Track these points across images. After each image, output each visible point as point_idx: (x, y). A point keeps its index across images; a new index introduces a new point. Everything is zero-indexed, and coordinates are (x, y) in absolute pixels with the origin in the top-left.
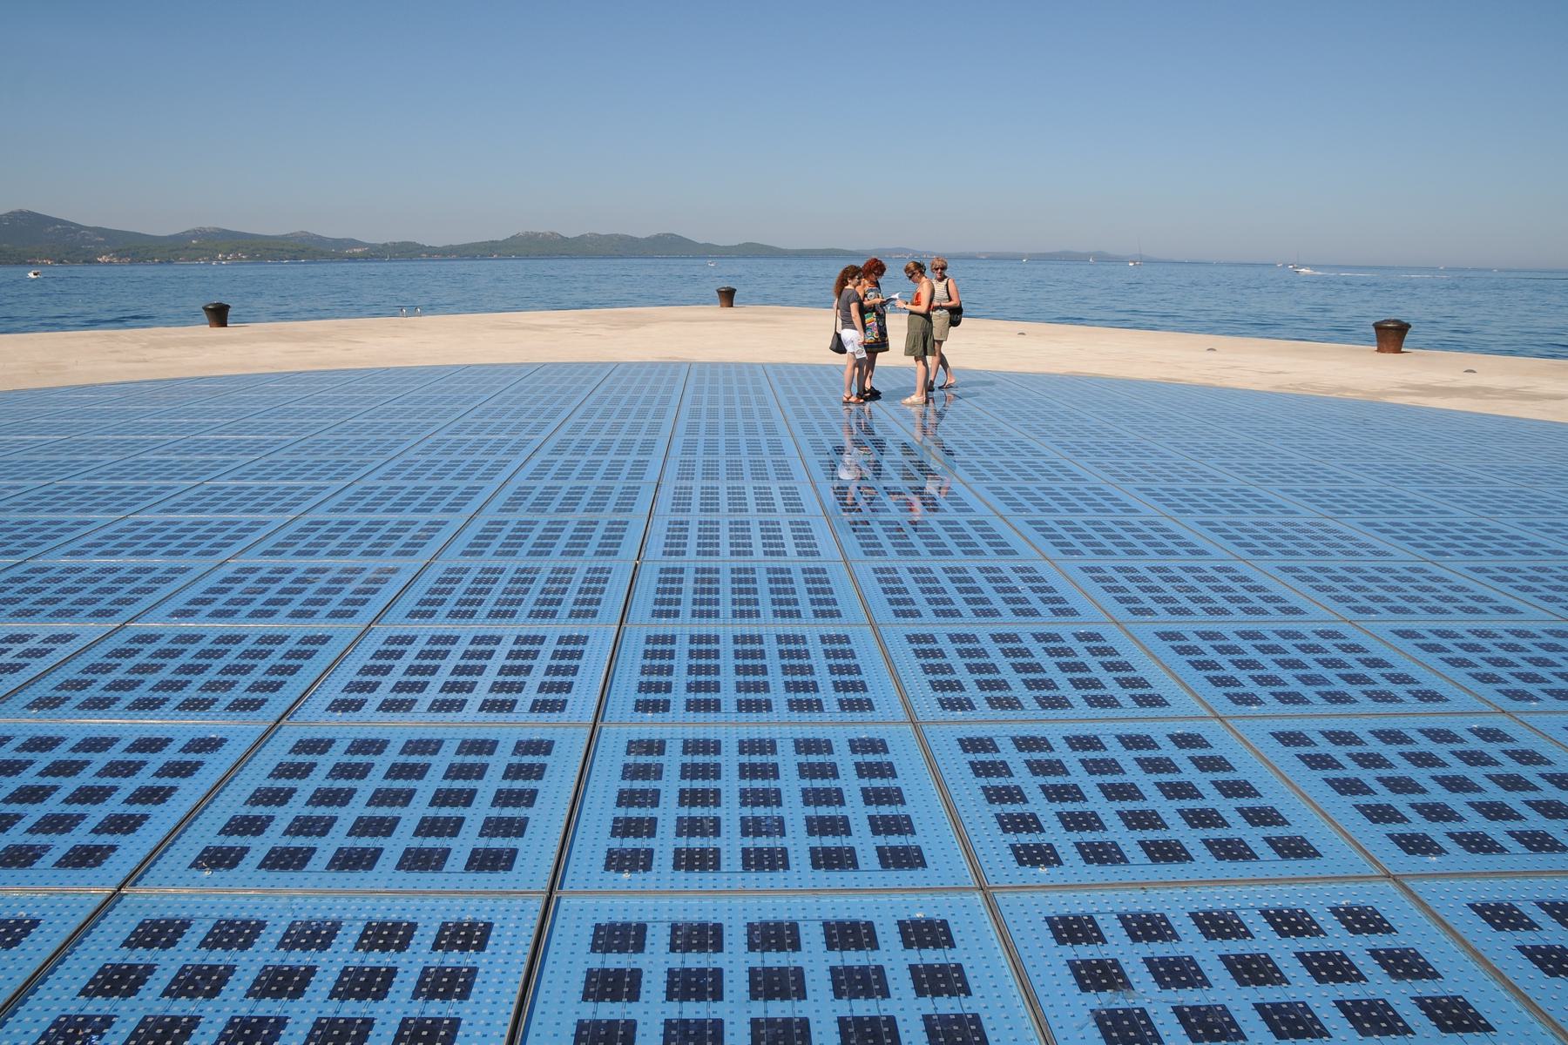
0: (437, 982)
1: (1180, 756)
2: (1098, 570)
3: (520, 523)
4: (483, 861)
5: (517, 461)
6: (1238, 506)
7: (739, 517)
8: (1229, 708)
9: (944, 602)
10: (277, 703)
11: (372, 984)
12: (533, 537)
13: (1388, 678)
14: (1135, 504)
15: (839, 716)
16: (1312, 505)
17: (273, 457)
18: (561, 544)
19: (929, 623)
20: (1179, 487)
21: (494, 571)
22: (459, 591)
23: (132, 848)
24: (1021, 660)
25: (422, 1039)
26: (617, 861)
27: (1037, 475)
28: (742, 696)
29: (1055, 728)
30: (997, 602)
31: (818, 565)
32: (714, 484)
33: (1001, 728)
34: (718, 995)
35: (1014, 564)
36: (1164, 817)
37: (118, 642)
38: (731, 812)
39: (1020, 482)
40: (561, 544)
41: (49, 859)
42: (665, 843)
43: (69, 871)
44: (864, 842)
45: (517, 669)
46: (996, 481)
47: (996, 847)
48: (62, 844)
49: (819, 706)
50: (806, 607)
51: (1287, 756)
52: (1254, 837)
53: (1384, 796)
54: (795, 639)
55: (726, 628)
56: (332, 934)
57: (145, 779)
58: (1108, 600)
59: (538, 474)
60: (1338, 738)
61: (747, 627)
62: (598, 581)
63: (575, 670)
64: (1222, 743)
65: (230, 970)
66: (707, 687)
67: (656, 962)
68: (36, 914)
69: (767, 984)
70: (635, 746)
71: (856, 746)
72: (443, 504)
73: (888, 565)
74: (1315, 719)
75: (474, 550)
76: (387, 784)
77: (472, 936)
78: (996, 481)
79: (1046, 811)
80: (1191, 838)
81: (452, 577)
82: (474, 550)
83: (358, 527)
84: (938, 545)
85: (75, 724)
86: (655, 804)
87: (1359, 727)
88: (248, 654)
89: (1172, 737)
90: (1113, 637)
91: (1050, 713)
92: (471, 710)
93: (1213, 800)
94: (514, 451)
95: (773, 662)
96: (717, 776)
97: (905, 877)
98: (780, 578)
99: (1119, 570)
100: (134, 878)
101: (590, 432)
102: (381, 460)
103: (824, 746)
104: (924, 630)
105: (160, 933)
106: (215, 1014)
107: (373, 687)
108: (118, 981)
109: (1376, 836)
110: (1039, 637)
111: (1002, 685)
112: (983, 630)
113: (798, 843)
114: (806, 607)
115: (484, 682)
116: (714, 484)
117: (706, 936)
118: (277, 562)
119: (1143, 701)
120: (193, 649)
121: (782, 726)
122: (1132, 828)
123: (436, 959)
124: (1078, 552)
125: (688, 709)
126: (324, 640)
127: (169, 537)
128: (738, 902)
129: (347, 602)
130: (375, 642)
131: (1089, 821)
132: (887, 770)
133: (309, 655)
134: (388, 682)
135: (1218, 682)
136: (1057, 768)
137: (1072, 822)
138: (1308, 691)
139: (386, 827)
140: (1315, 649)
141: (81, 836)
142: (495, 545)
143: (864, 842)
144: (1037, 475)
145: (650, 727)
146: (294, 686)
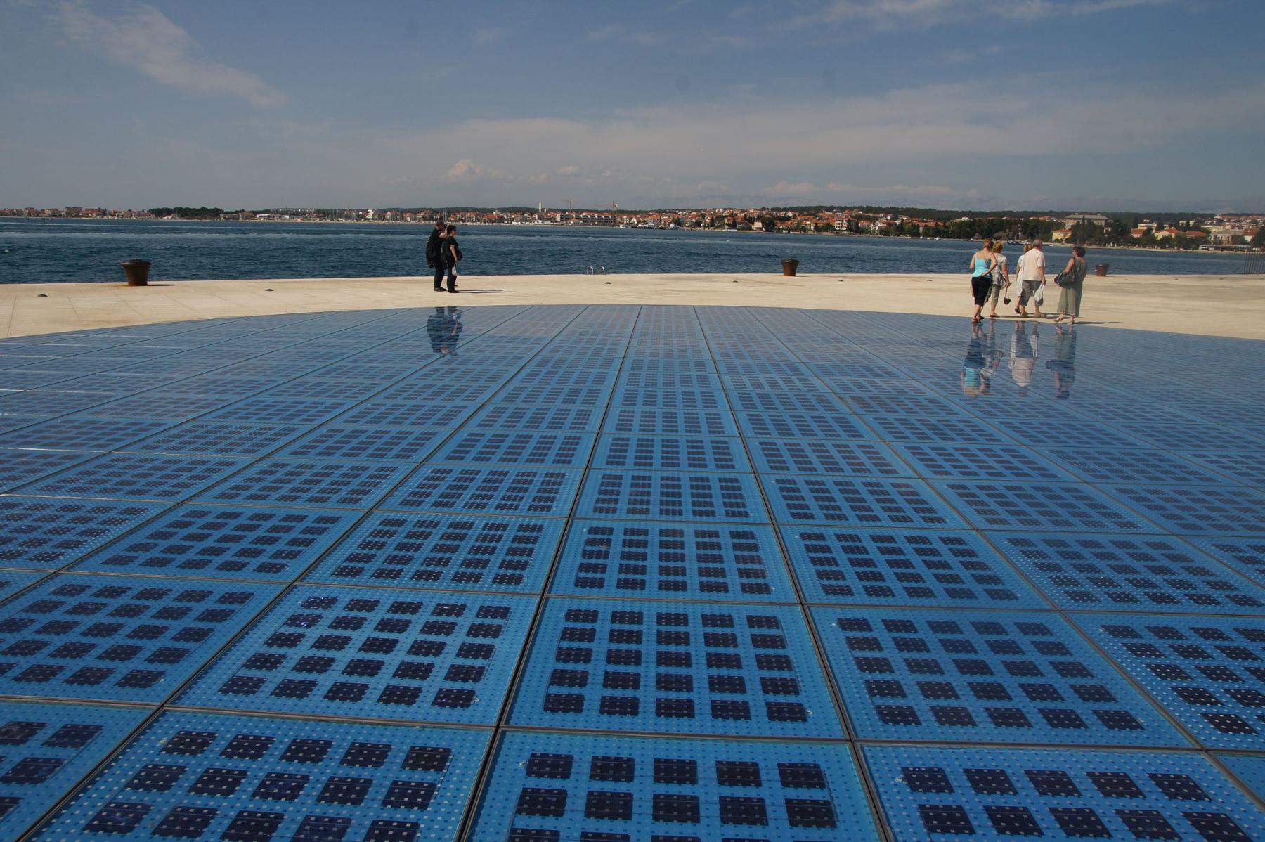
0: (338, 788)
1: (1023, 640)
2: (964, 487)
3: (495, 436)
4: (446, 699)
5: (494, 387)
6: (1063, 437)
7: (694, 437)
8: (1068, 603)
9: (834, 508)
10: (293, 569)
11: (288, 788)
12: (530, 447)
13: (1209, 583)
14: (998, 435)
15: (741, 596)
16: (1149, 439)
17: (303, 379)
18: (526, 454)
19: (819, 524)
20: (1035, 422)
21: (472, 472)
22: (443, 487)
23: (174, 675)
24: (895, 557)
25: (402, 838)
26: (554, 704)
27: (917, 409)
28: (664, 578)
29: (920, 614)
30: (877, 510)
31: (733, 476)
32: (672, 410)
33: (875, 613)
34: (627, 816)
35: (864, 480)
36: (1061, 691)
37: (178, 515)
38: (649, 670)
39: (903, 414)
40: (526, 454)
41: (113, 679)
42: (594, 692)
43: (127, 689)
44: (756, 698)
45: (484, 549)
46: (883, 414)
47: (863, 708)
48: (123, 668)
49: (724, 588)
50: (719, 509)
51: (1115, 645)
52: (1084, 709)
53: (1201, 682)
54: (745, 535)
55: (654, 524)
56: (324, 751)
57: (188, 622)
58: (970, 511)
59: (511, 398)
60: (1209, 634)
61: (638, 522)
62: (554, 483)
63: (530, 552)
64: (1062, 630)
65: (243, 774)
66: (636, 570)
67: (578, 786)
68: (99, 722)
69: (598, 806)
70: (573, 615)
71: (753, 621)
72: (434, 419)
73: (789, 478)
74: (1143, 616)
75: (457, 456)
76: (376, 635)
77: (434, 759)
78: (883, 414)
79: (908, 680)
80: (1031, 709)
81: (440, 474)
82: (457, 456)
83: (343, 434)
84: (806, 463)
85: (137, 577)
86: (638, 663)
87: (1180, 624)
88: (274, 529)
89: (974, 624)
90: (974, 541)
91: (916, 601)
92: (486, 583)
93: (1051, 678)
94: (492, 379)
95: (728, 553)
96: (639, 641)
97: (789, 728)
98: (700, 486)
99: (1009, 488)
100: (176, 697)
101: (571, 366)
102: (389, 383)
103: (727, 621)
104: (850, 531)
105: (191, 743)
106: (364, 815)
107: (370, 558)
108: (157, 778)
109: (1192, 716)
110: (911, 540)
111: (878, 577)
112: (865, 532)
113: (702, 697)
114: (719, 509)
115: (458, 558)
116: (672, 410)
117: (682, 771)
118: (303, 460)
119: (994, 595)
120: (267, 525)
121: (693, 604)
122: (927, 696)
123: (405, 776)
124: (947, 473)
125: (618, 587)
126: (333, 520)
127: (197, 437)
128: (650, 744)
129: (353, 492)
130: (374, 523)
131: (997, 692)
132: (778, 642)
133: (322, 531)
134: (382, 554)
135: (1058, 582)
136: (920, 645)
137: (982, 691)
138: (1176, 593)
139: (372, 669)
140: (1145, 557)
141: (137, 663)
142: (500, 453)
143: (756, 698)
144: (917, 409)
145: (587, 600)
146: (309, 555)
